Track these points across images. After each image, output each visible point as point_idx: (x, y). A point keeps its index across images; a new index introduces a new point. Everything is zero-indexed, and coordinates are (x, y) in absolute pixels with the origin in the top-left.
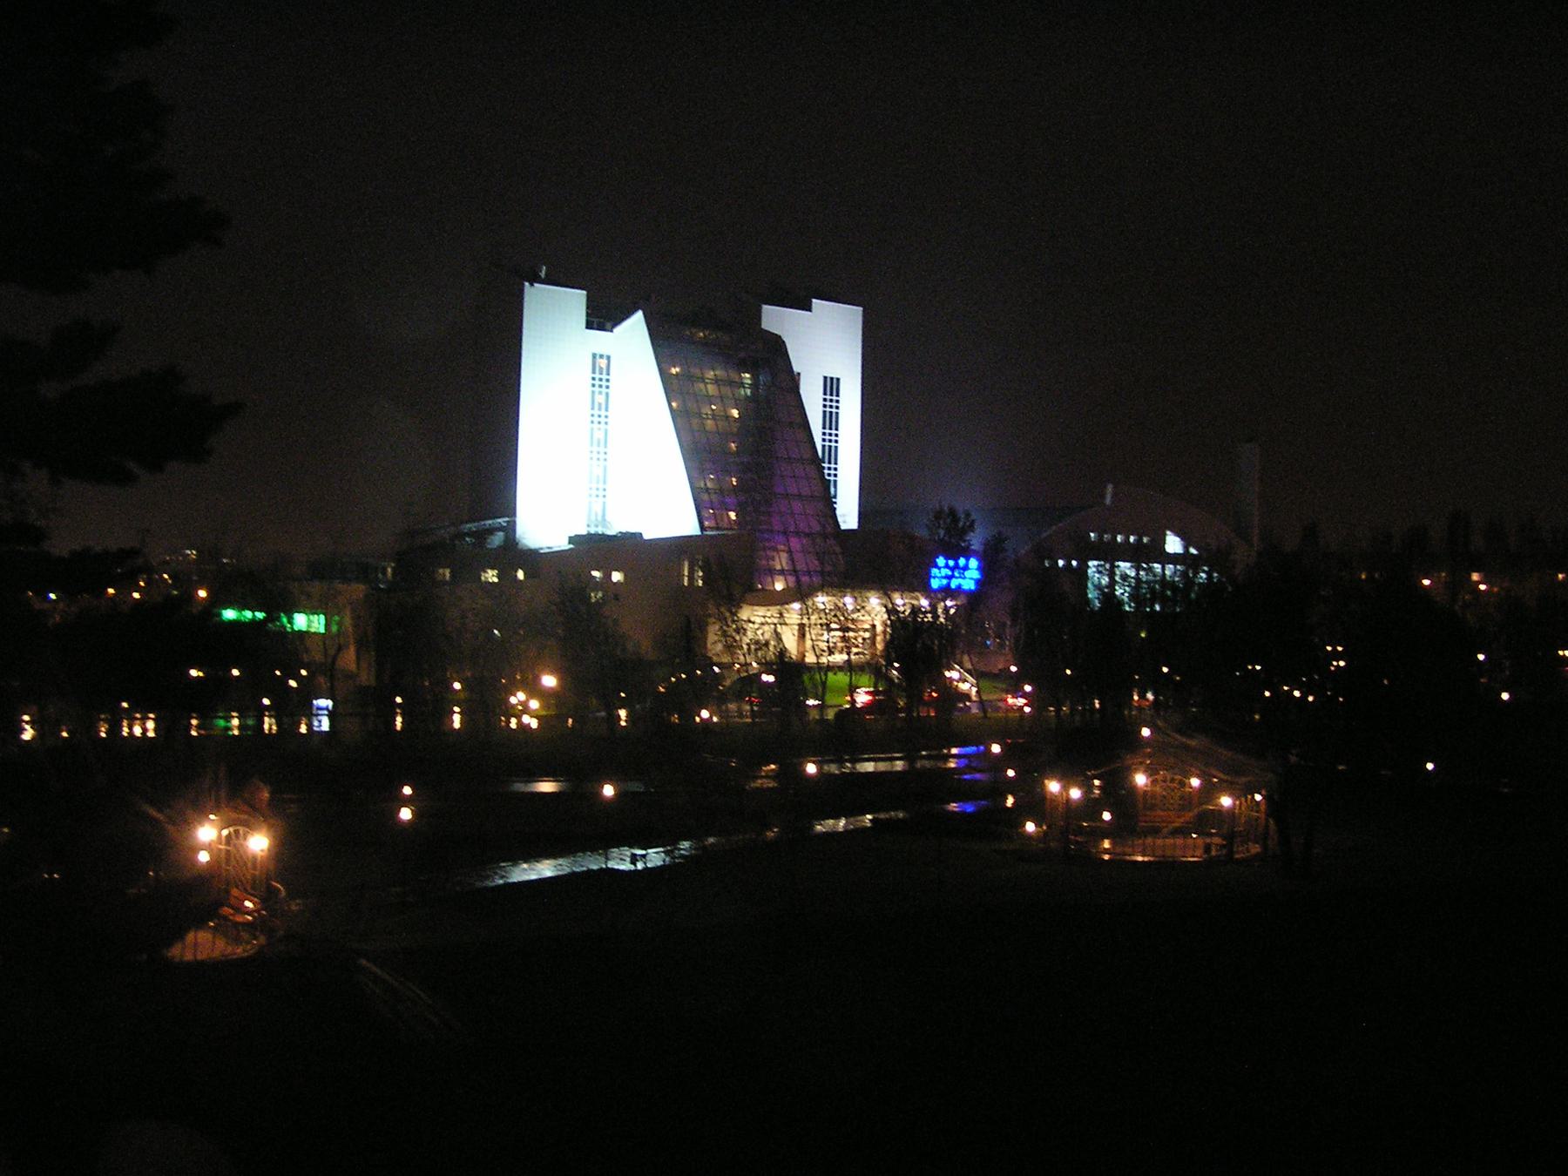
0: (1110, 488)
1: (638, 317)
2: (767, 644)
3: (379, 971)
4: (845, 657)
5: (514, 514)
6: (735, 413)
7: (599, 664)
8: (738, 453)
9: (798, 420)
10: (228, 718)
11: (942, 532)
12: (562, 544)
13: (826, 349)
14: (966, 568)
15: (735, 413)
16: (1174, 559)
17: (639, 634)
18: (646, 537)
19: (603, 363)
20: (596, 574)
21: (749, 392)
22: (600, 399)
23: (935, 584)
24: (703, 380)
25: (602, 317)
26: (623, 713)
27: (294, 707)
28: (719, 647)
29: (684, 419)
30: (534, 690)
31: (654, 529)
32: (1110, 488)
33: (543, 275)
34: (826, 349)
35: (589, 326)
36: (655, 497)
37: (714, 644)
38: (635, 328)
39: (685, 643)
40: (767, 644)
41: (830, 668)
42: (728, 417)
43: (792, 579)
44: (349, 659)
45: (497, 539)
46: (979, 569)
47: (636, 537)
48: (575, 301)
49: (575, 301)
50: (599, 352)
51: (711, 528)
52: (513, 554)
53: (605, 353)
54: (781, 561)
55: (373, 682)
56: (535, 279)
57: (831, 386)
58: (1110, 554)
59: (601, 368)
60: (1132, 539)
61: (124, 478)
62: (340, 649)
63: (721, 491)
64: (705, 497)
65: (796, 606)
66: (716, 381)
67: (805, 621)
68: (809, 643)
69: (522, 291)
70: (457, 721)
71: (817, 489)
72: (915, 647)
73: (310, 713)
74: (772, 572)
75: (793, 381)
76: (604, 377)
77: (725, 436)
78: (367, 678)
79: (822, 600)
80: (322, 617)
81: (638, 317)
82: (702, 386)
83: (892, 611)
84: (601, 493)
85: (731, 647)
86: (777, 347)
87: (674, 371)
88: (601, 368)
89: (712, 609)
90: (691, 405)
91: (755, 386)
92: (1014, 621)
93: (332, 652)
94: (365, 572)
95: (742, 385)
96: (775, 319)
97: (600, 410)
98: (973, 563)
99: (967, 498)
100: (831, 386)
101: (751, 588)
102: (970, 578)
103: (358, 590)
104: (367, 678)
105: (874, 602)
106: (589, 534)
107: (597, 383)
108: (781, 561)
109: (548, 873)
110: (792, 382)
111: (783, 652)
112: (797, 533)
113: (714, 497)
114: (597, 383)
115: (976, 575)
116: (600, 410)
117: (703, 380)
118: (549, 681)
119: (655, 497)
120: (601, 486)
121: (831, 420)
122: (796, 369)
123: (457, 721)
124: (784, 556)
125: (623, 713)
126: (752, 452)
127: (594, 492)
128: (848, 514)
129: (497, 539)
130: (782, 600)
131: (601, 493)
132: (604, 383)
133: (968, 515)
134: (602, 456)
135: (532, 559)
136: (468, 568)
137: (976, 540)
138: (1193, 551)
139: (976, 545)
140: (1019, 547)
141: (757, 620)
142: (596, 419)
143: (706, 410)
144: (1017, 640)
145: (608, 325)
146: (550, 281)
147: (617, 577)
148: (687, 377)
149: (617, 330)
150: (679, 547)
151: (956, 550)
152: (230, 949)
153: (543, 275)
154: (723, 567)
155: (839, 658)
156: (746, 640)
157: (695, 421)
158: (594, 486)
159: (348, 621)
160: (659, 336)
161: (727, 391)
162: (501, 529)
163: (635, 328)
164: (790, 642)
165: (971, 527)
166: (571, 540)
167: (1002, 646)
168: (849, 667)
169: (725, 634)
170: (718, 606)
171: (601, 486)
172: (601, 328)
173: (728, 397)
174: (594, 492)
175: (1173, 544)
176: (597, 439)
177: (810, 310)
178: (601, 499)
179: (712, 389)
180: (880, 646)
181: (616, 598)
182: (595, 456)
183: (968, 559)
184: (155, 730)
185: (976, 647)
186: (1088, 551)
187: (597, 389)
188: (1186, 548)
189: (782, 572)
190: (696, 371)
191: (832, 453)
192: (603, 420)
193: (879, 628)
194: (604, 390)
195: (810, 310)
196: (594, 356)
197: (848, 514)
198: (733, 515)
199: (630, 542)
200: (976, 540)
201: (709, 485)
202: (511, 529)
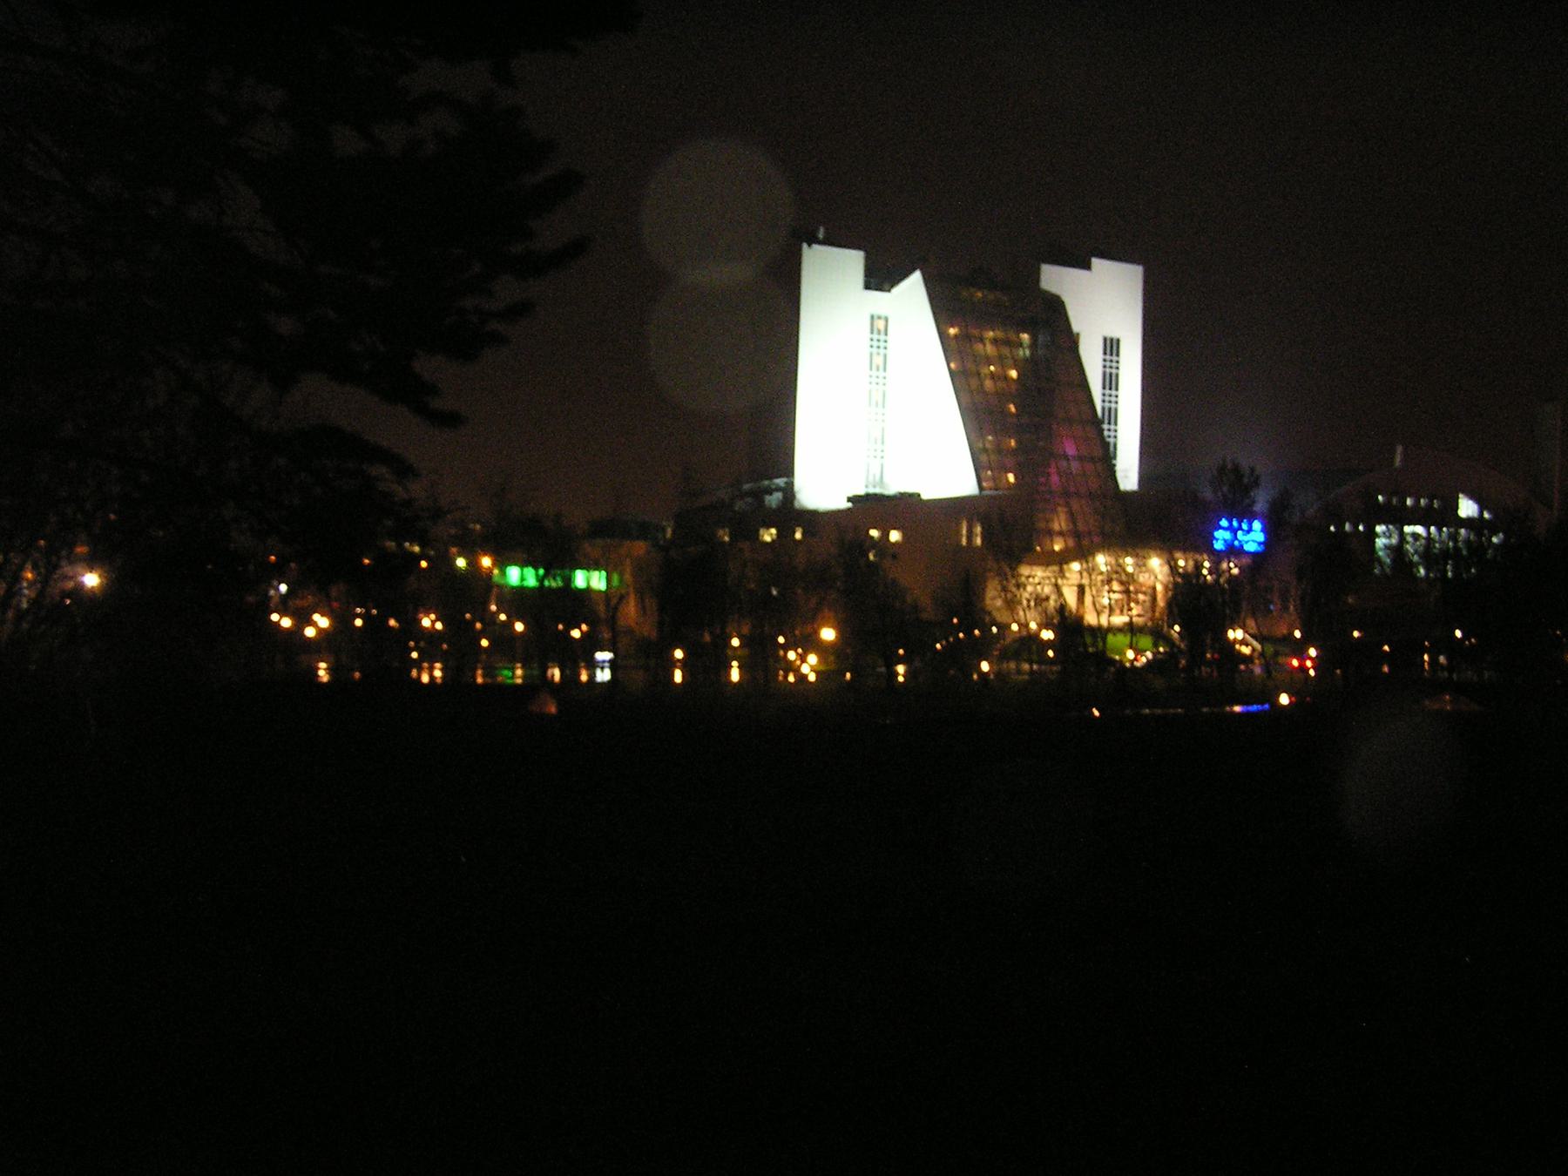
0: (1399, 449)
1: (917, 277)
2: (1047, 598)
4: (1126, 619)
6: (1014, 374)
7: (878, 618)
8: (1017, 415)
10: (513, 669)
11: (1225, 489)
12: (845, 505)
13: (1106, 310)
14: (1250, 530)
15: (1014, 374)
16: (1468, 523)
17: (918, 588)
19: (880, 324)
20: (874, 533)
21: (1028, 352)
22: (878, 360)
23: (1219, 545)
24: (982, 340)
25: (880, 277)
26: (901, 669)
27: (582, 654)
28: (999, 603)
29: (960, 378)
30: (433, 622)
31: (931, 491)
32: (1399, 449)
33: (821, 236)
34: (1106, 310)
35: (868, 287)
36: (931, 455)
37: (993, 599)
38: (913, 287)
39: (969, 608)
40: (1047, 598)
41: (1111, 629)
42: (1006, 378)
43: (1071, 543)
44: (631, 609)
45: (774, 500)
46: (1263, 530)
47: (914, 497)
49: (853, 262)
50: (876, 313)
52: (789, 514)
53: (883, 313)
54: (1060, 522)
55: (654, 635)
56: (813, 240)
58: (1398, 518)
59: (879, 327)
62: (622, 598)
64: (984, 458)
65: (1076, 566)
66: (995, 341)
67: (1085, 581)
68: (1088, 599)
69: (800, 250)
70: (735, 675)
71: (1098, 452)
72: (1196, 606)
73: (593, 665)
74: (1050, 533)
75: (1072, 342)
77: (1003, 397)
78: (648, 630)
79: (1102, 560)
80: (604, 573)
81: (917, 277)
82: (980, 346)
83: (1173, 569)
84: (879, 454)
85: (1012, 604)
87: (952, 331)
88: (879, 327)
89: (990, 564)
90: (971, 366)
91: (1034, 345)
92: (1300, 579)
93: (614, 601)
94: (645, 531)
95: (1021, 345)
96: (1056, 279)
97: (879, 362)
98: (1257, 525)
99: (1254, 456)
100: (1111, 347)
101: (1031, 549)
102: (1253, 538)
103: (640, 547)
104: (648, 630)
105: (1156, 563)
106: (868, 495)
108: (1060, 522)
110: (1070, 343)
111: (1062, 608)
112: (1077, 494)
113: (993, 457)
115: (1261, 537)
116: (879, 362)
117: (982, 340)
119: (931, 455)
121: (1111, 381)
122: (1076, 328)
123: (735, 675)
124: (1063, 517)
125: (901, 669)
126: (1026, 403)
128: (1128, 475)
129: (774, 500)
130: (1061, 560)
131: (879, 454)
133: (1252, 470)
135: (812, 519)
136: (746, 530)
137: (1261, 503)
138: (1486, 515)
139: (1260, 506)
140: (1307, 504)
141: (1036, 578)
143: (984, 371)
144: (1302, 599)
146: (830, 241)
147: (895, 536)
148: (965, 337)
149: (895, 290)
150: (954, 508)
151: (1244, 513)
153: (821, 236)
154: (1006, 526)
155: (1119, 620)
156: (1026, 595)
157: (974, 382)
159: (628, 577)
160: (944, 307)
161: (1006, 351)
162: (778, 489)
163: (913, 287)
164: (1071, 597)
165: (1256, 483)
167: (1286, 608)
168: (1131, 628)
169: (1005, 589)
170: (997, 561)
173: (1009, 357)
175: (1467, 508)
176: (874, 400)
179: (990, 349)
180: (1161, 603)
185: (1260, 609)
186: (1377, 514)
187: (875, 350)
188: (1481, 513)
189: (1061, 534)
190: (976, 332)
191: (1112, 415)
192: (882, 344)
193: (1159, 588)
194: (882, 351)
197: (1128, 475)
198: (1011, 478)
200: (1261, 503)
201: (988, 446)
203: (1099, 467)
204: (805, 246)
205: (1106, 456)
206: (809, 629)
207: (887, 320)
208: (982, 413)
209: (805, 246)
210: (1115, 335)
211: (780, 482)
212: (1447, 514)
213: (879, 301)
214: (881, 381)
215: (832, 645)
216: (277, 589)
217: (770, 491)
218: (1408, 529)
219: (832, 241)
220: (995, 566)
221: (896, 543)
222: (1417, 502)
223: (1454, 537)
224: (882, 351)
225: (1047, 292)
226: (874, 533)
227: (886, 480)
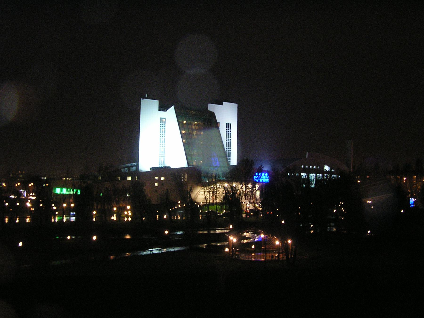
1: (173, 107)
3: (352, 162)
9: (177, 110)
12: (148, 170)
16: (327, 172)
19: (164, 120)
25: (163, 108)
30: (128, 210)
31: (173, 166)
35: (160, 110)
36: (176, 158)
38: (172, 110)
48: (155, 103)
49: (155, 103)
50: (162, 117)
56: (144, 97)
57: (229, 126)
58: (308, 172)
59: (163, 121)
60: (314, 167)
61: (151, 169)
70: (94, 220)
76: (164, 124)
81: (173, 107)
86: (212, 115)
88: (163, 121)
96: (212, 107)
97: (163, 132)
100: (229, 126)
109: (176, 250)
114: (162, 126)
116: (163, 132)
120: (163, 154)
121: (229, 135)
122: (218, 121)
123: (94, 220)
127: (161, 156)
129: (134, 168)
131: (163, 156)
132: (164, 126)
134: (163, 146)
142: (162, 136)
152: (135, 254)
158: (161, 154)
160: (179, 115)
162: (135, 166)
163: (172, 110)
166: (151, 169)
171: (163, 154)
172: (163, 110)
174: (161, 156)
175: (327, 168)
176: (160, 141)
177: (222, 105)
181: (162, 184)
182: (161, 146)
183: (262, 173)
187: (162, 127)
192: (164, 126)
195: (222, 105)
196: (161, 118)
199: (167, 169)
202: (137, 166)
204: (142, 99)
209: (142, 99)
211: (135, 164)
214: (163, 136)
215: (71, 207)
216: (6, 202)
217: (132, 166)
218: (318, 174)
220: (229, 190)
222: (317, 167)
224: (164, 127)
225: (210, 111)
227: (165, 163)
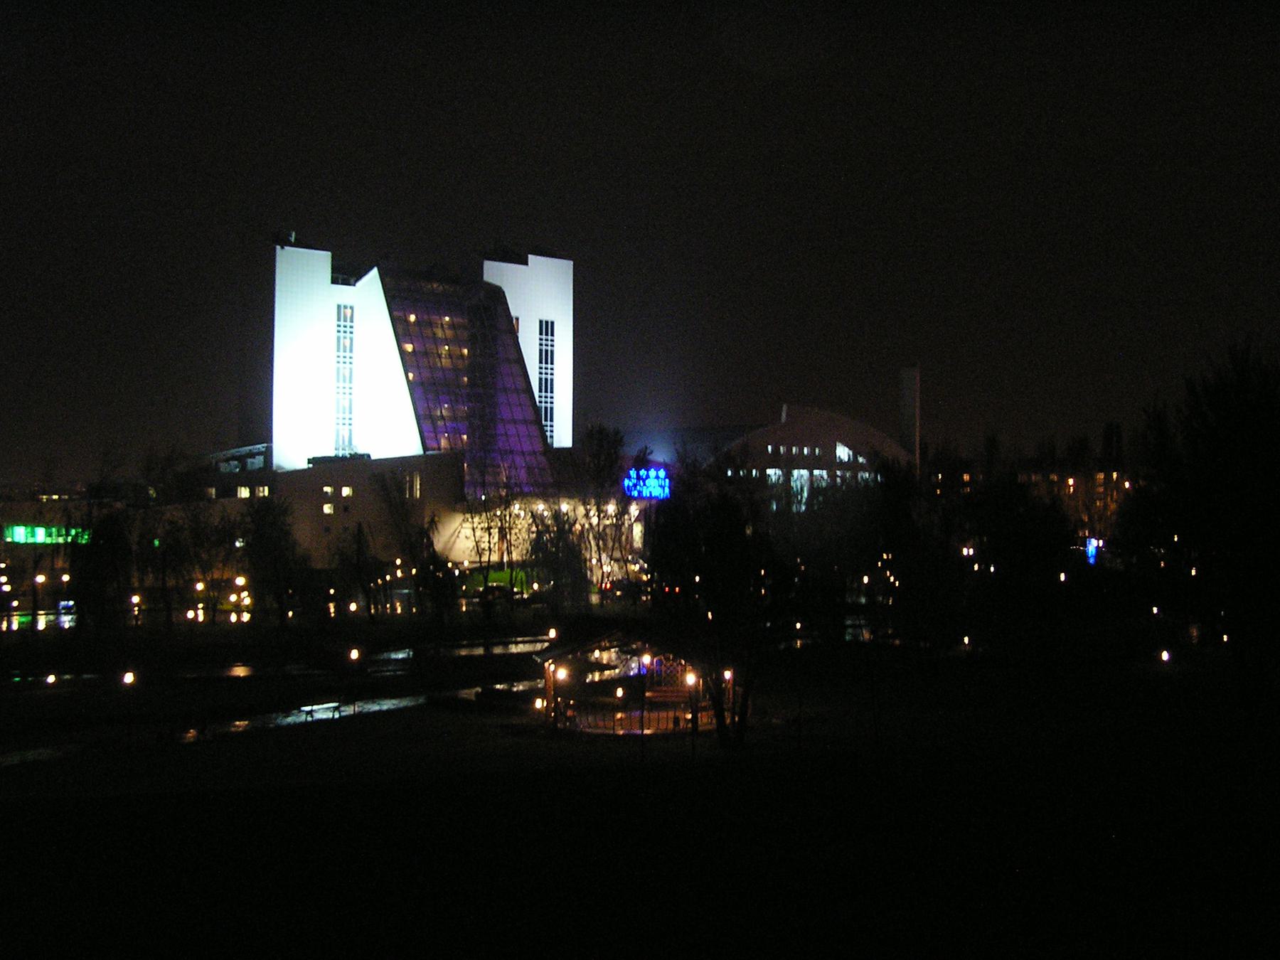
0: (785, 408)
1: (374, 272)
5: (271, 441)
13: (541, 298)
14: (648, 477)
18: (373, 457)
19: (349, 311)
25: (345, 274)
29: (408, 361)
30: (239, 590)
31: (379, 452)
33: (293, 239)
34: (541, 298)
35: (334, 281)
36: (389, 428)
48: (321, 260)
49: (321, 260)
51: (253, 455)
56: (285, 243)
57: (547, 328)
59: (344, 315)
63: (454, 418)
76: (348, 324)
81: (374, 272)
84: (347, 422)
86: (497, 296)
88: (344, 315)
96: (496, 272)
97: (345, 347)
100: (547, 328)
107: (342, 329)
116: (345, 347)
118: (240, 581)
119: (389, 428)
120: (347, 416)
121: (546, 357)
122: (513, 313)
127: (341, 421)
131: (347, 422)
132: (348, 330)
134: (347, 391)
145: (352, 281)
146: (299, 244)
147: (346, 491)
149: (359, 284)
158: (341, 416)
162: (259, 453)
166: (310, 461)
171: (347, 416)
174: (341, 421)
175: (843, 452)
176: (337, 376)
177: (526, 263)
178: (347, 427)
183: (648, 470)
184: (593, 682)
187: (342, 334)
192: (348, 330)
195: (526, 263)
196: (339, 307)
197: (562, 434)
202: (268, 454)
203: (533, 428)
205: (539, 418)
206: (27, 582)
207: (352, 308)
208: (428, 388)
210: (550, 319)
211: (261, 447)
212: (830, 462)
213: (344, 293)
219: (305, 242)
221: (348, 497)
223: (832, 476)
224: (348, 335)
226: (327, 489)
227: (354, 443)
